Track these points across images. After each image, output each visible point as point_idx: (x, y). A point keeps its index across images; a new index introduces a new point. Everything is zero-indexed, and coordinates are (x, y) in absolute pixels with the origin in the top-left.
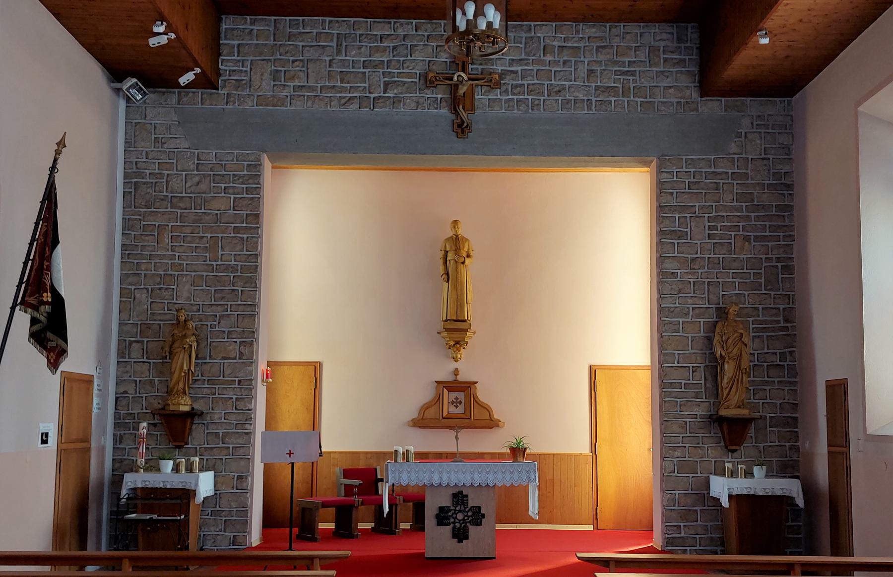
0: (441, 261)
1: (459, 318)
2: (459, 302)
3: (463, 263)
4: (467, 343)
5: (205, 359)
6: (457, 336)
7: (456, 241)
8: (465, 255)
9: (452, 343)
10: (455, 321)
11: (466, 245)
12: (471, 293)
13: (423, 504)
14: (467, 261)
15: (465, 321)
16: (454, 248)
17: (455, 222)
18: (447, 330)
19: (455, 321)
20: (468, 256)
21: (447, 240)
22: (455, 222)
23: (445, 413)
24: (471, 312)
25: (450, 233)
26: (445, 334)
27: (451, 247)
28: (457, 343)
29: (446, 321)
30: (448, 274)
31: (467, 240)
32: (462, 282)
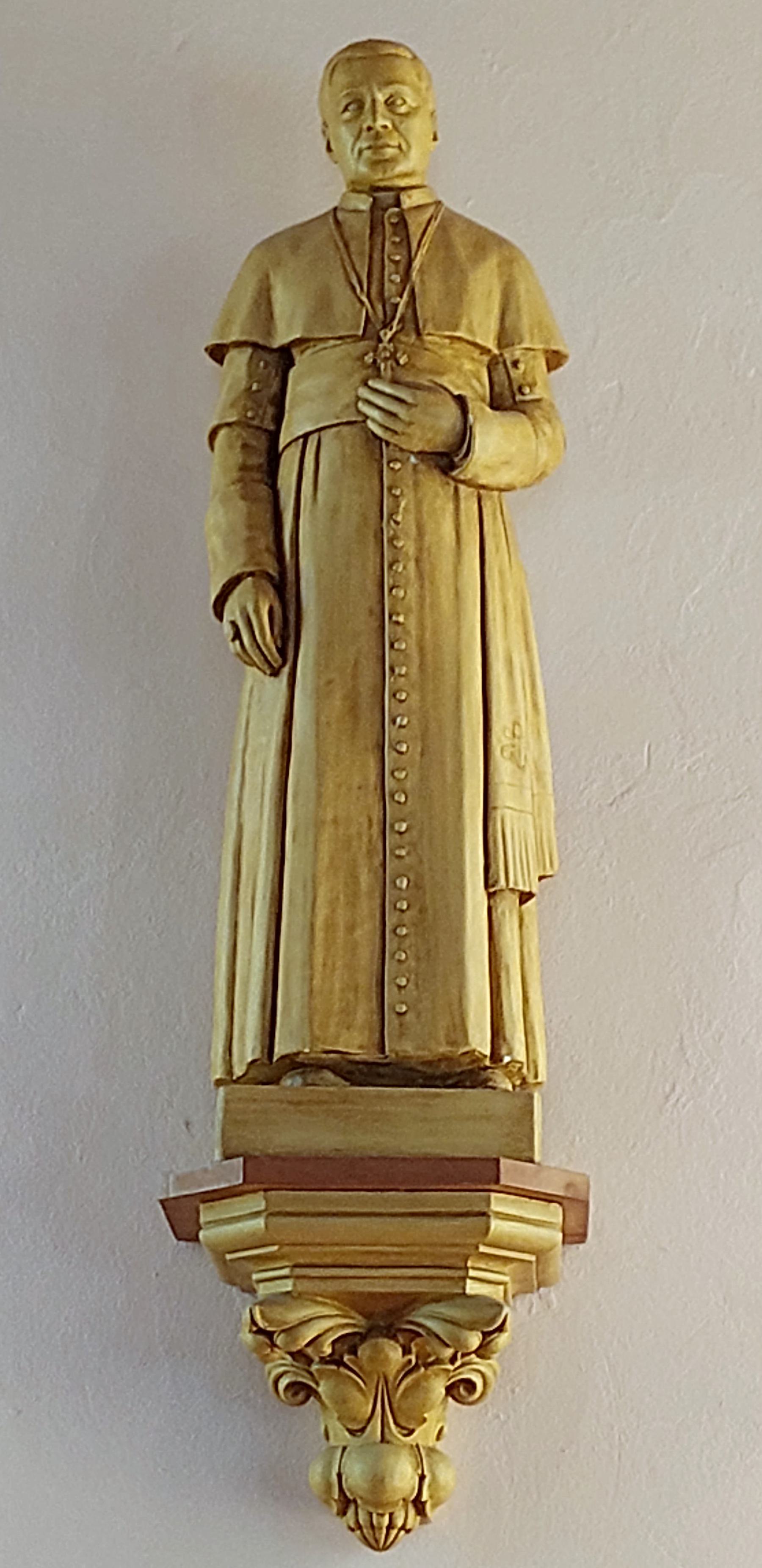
0: (214, 471)
1: (405, 1047)
2: (396, 852)
3: (449, 459)
4: (489, 1321)
5: (456, 328)
6: (376, 1230)
7: (383, 255)
8: (470, 379)
9: (323, 1323)
10: (356, 1073)
11: (484, 285)
12: (530, 791)
13: (263, 243)
14: (496, 443)
15: (470, 1075)
16: (348, 312)
17: (367, 66)
18: (266, 1173)
19: (356, 1073)
20: (507, 399)
21: (295, 238)
22: (367, 66)
23: (248, 1049)
24: (567, 988)
25: (319, 187)
26: (241, 1221)
27: (322, 305)
28: (386, 1318)
29: (271, 1068)
30: (283, 584)
31: (485, 242)
32: (434, 671)
